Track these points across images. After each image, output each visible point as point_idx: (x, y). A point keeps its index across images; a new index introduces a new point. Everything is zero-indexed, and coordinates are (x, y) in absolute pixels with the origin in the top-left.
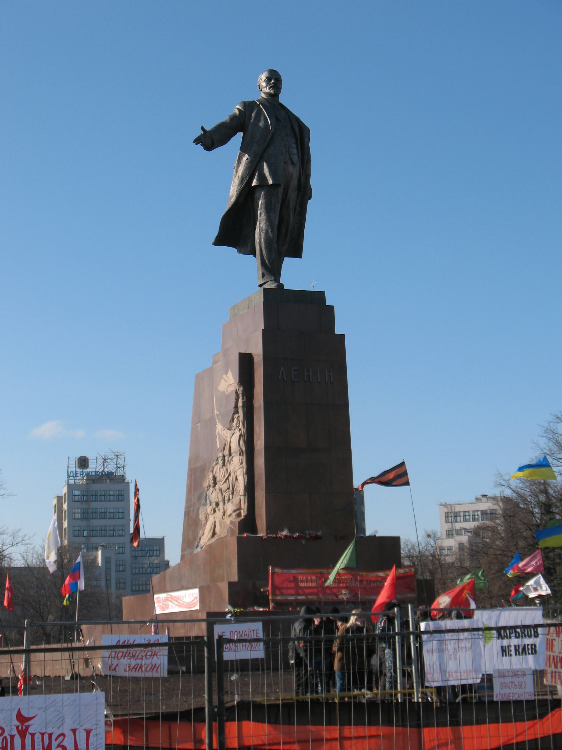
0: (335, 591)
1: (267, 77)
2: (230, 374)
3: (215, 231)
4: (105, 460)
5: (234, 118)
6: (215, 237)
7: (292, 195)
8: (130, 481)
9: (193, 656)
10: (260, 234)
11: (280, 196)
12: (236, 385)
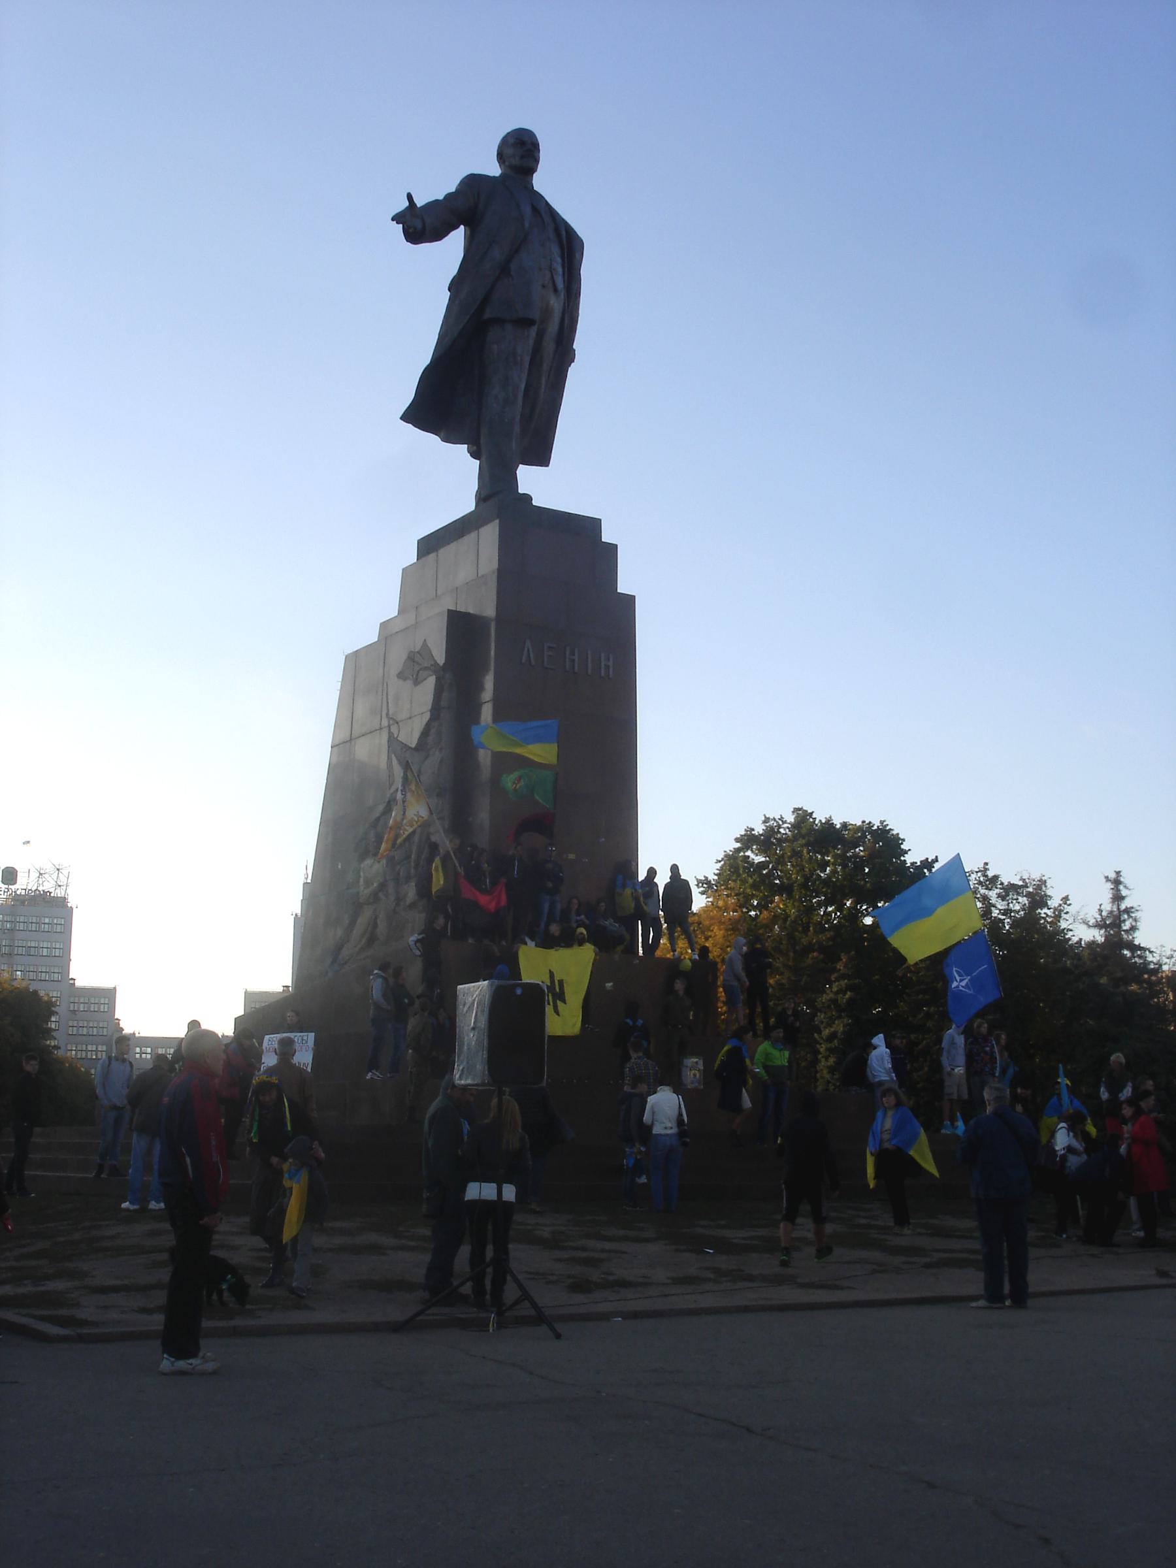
3: (407, 395)
4: (41, 874)
7: (549, 345)
11: (531, 342)
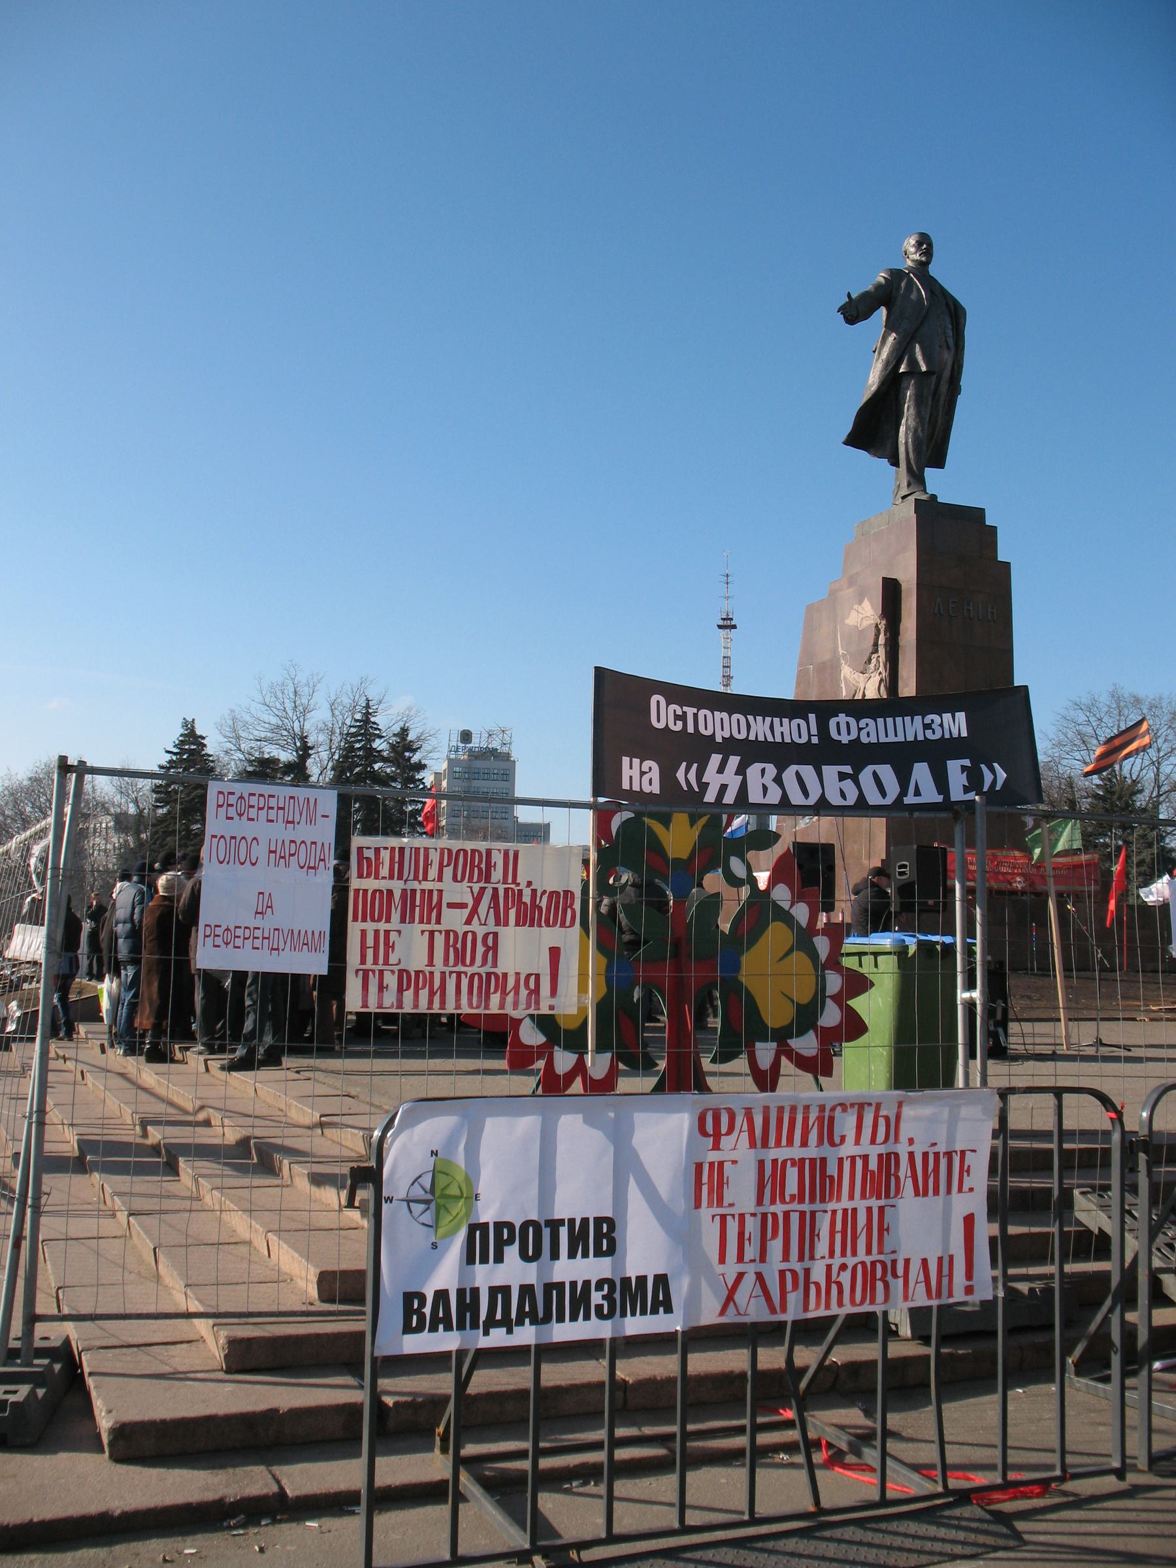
0: (1009, 877)
1: (917, 242)
2: (866, 604)
3: (848, 427)
5: (879, 287)
6: (847, 434)
7: (944, 388)
8: (516, 760)
9: (969, 952)
10: (906, 433)
11: (933, 387)
12: (876, 617)
